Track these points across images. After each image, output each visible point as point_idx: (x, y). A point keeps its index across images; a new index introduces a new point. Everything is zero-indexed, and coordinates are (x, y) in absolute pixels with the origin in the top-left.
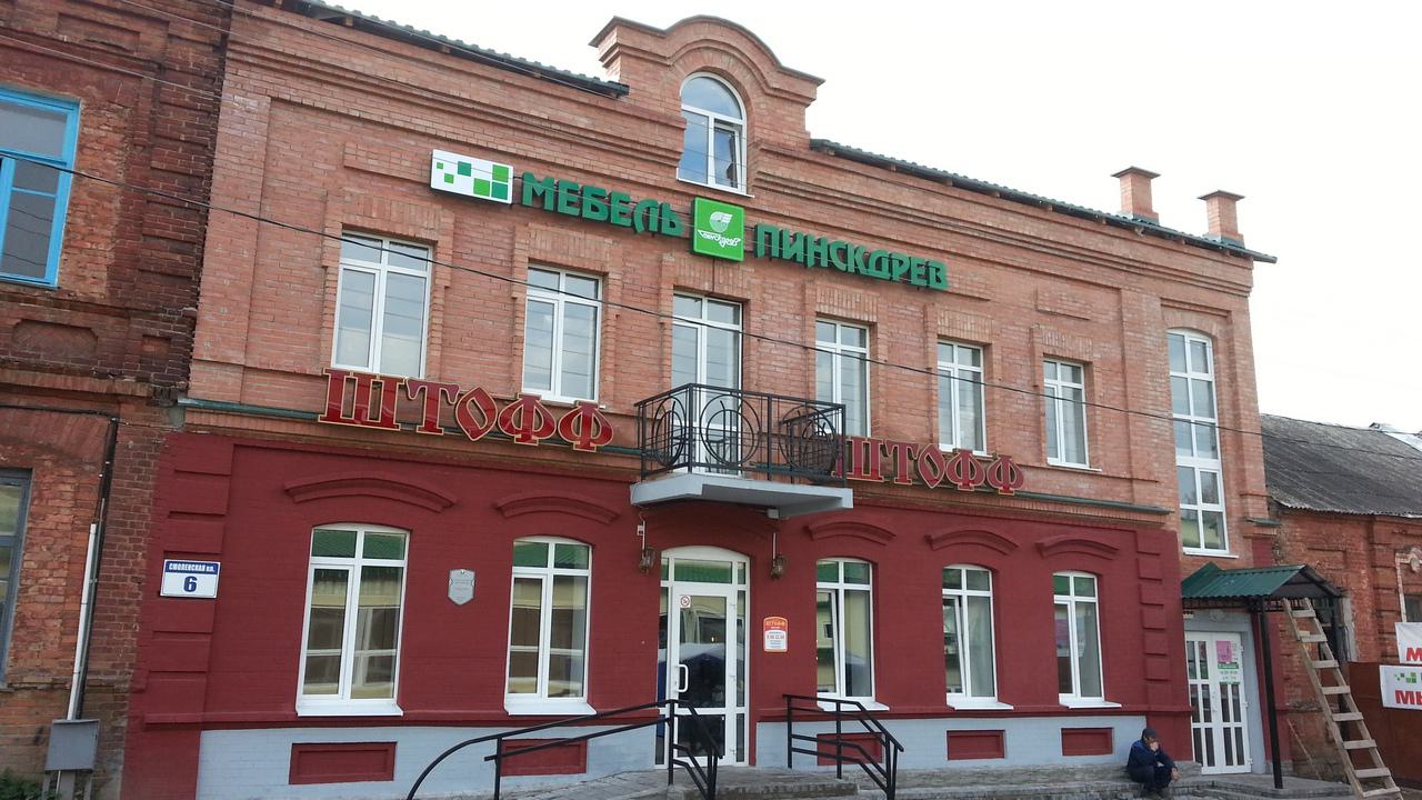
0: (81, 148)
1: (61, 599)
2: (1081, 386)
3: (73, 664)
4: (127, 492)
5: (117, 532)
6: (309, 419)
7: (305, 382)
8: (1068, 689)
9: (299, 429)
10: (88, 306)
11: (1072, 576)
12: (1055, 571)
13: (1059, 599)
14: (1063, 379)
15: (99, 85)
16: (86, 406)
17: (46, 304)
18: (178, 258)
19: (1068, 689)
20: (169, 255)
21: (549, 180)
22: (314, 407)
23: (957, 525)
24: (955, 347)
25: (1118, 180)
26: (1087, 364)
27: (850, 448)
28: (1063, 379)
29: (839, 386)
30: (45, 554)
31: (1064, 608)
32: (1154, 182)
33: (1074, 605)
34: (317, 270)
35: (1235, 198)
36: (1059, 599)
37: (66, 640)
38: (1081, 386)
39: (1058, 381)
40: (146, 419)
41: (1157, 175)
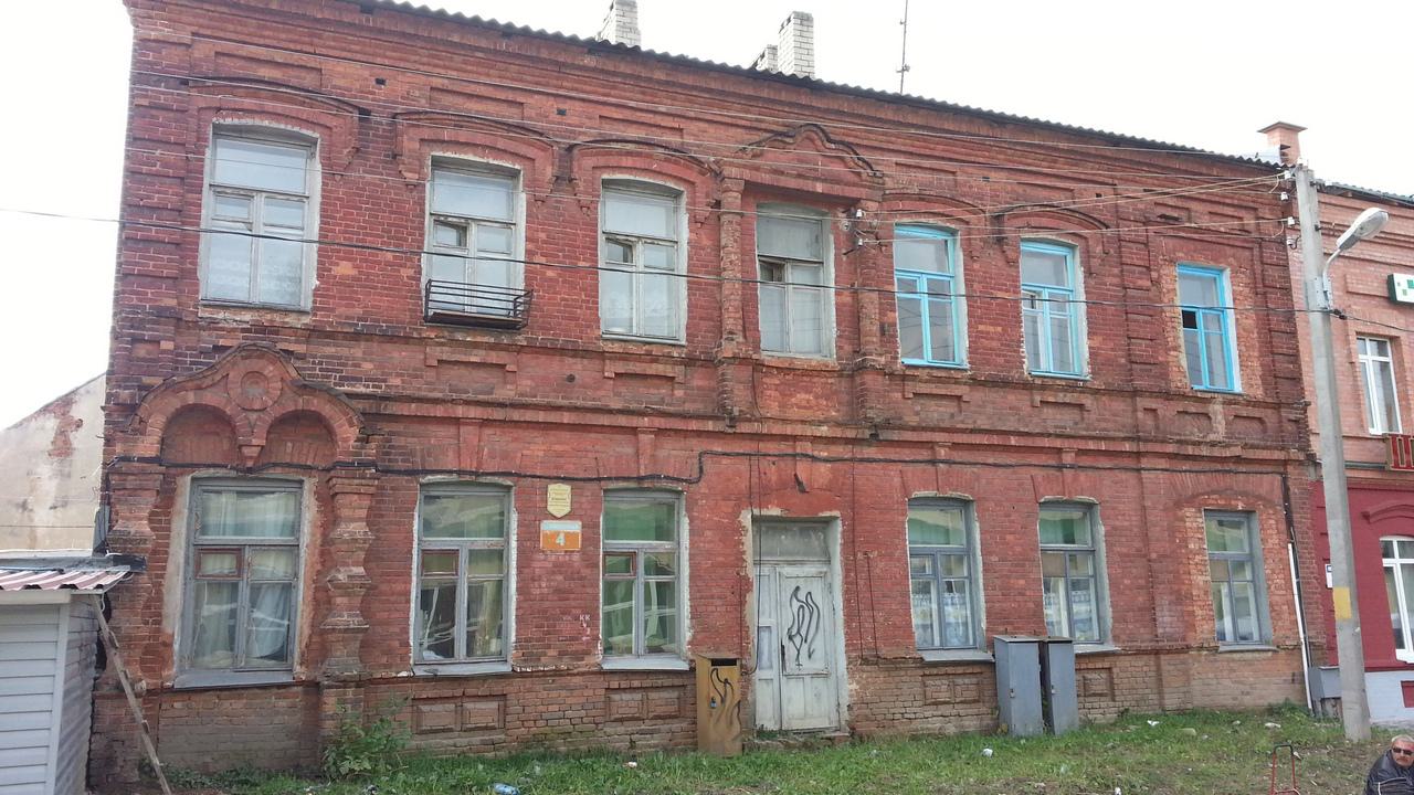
0: (1234, 300)
1: (1284, 592)
2: (1389, 359)
3: (1298, 632)
4: (1301, 522)
5: (1303, 548)
6: (1380, 468)
7: (1356, 442)
8: (1401, 645)
9: (1370, 475)
10: (1072, 385)
11: (1395, 540)
12: (1382, 536)
13: (1387, 562)
14: (1372, 354)
15: (1233, 256)
16: (1269, 469)
17: (1243, 405)
18: (1291, 366)
19: (1401, 645)
20: (1286, 365)
21: (427, 174)
22: (1383, 459)
23: (1392, 501)
24: (1368, 342)
25: (1266, 135)
26: (1393, 339)
27: (1400, 444)
28: (1372, 354)
29: (929, 349)
30: (1272, 566)
31: (1389, 570)
32: (1301, 134)
33: (1399, 566)
34: (1347, 365)
35: (1295, 130)
36: (1387, 562)
37: (1293, 618)
38: (1389, 359)
39: (1369, 357)
40: (1299, 474)
41: (1304, 129)
